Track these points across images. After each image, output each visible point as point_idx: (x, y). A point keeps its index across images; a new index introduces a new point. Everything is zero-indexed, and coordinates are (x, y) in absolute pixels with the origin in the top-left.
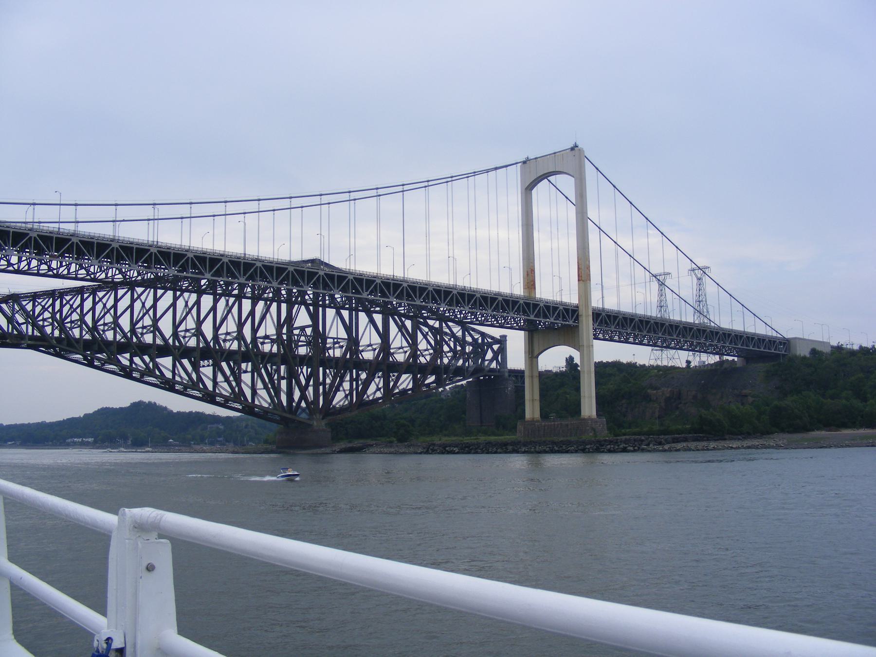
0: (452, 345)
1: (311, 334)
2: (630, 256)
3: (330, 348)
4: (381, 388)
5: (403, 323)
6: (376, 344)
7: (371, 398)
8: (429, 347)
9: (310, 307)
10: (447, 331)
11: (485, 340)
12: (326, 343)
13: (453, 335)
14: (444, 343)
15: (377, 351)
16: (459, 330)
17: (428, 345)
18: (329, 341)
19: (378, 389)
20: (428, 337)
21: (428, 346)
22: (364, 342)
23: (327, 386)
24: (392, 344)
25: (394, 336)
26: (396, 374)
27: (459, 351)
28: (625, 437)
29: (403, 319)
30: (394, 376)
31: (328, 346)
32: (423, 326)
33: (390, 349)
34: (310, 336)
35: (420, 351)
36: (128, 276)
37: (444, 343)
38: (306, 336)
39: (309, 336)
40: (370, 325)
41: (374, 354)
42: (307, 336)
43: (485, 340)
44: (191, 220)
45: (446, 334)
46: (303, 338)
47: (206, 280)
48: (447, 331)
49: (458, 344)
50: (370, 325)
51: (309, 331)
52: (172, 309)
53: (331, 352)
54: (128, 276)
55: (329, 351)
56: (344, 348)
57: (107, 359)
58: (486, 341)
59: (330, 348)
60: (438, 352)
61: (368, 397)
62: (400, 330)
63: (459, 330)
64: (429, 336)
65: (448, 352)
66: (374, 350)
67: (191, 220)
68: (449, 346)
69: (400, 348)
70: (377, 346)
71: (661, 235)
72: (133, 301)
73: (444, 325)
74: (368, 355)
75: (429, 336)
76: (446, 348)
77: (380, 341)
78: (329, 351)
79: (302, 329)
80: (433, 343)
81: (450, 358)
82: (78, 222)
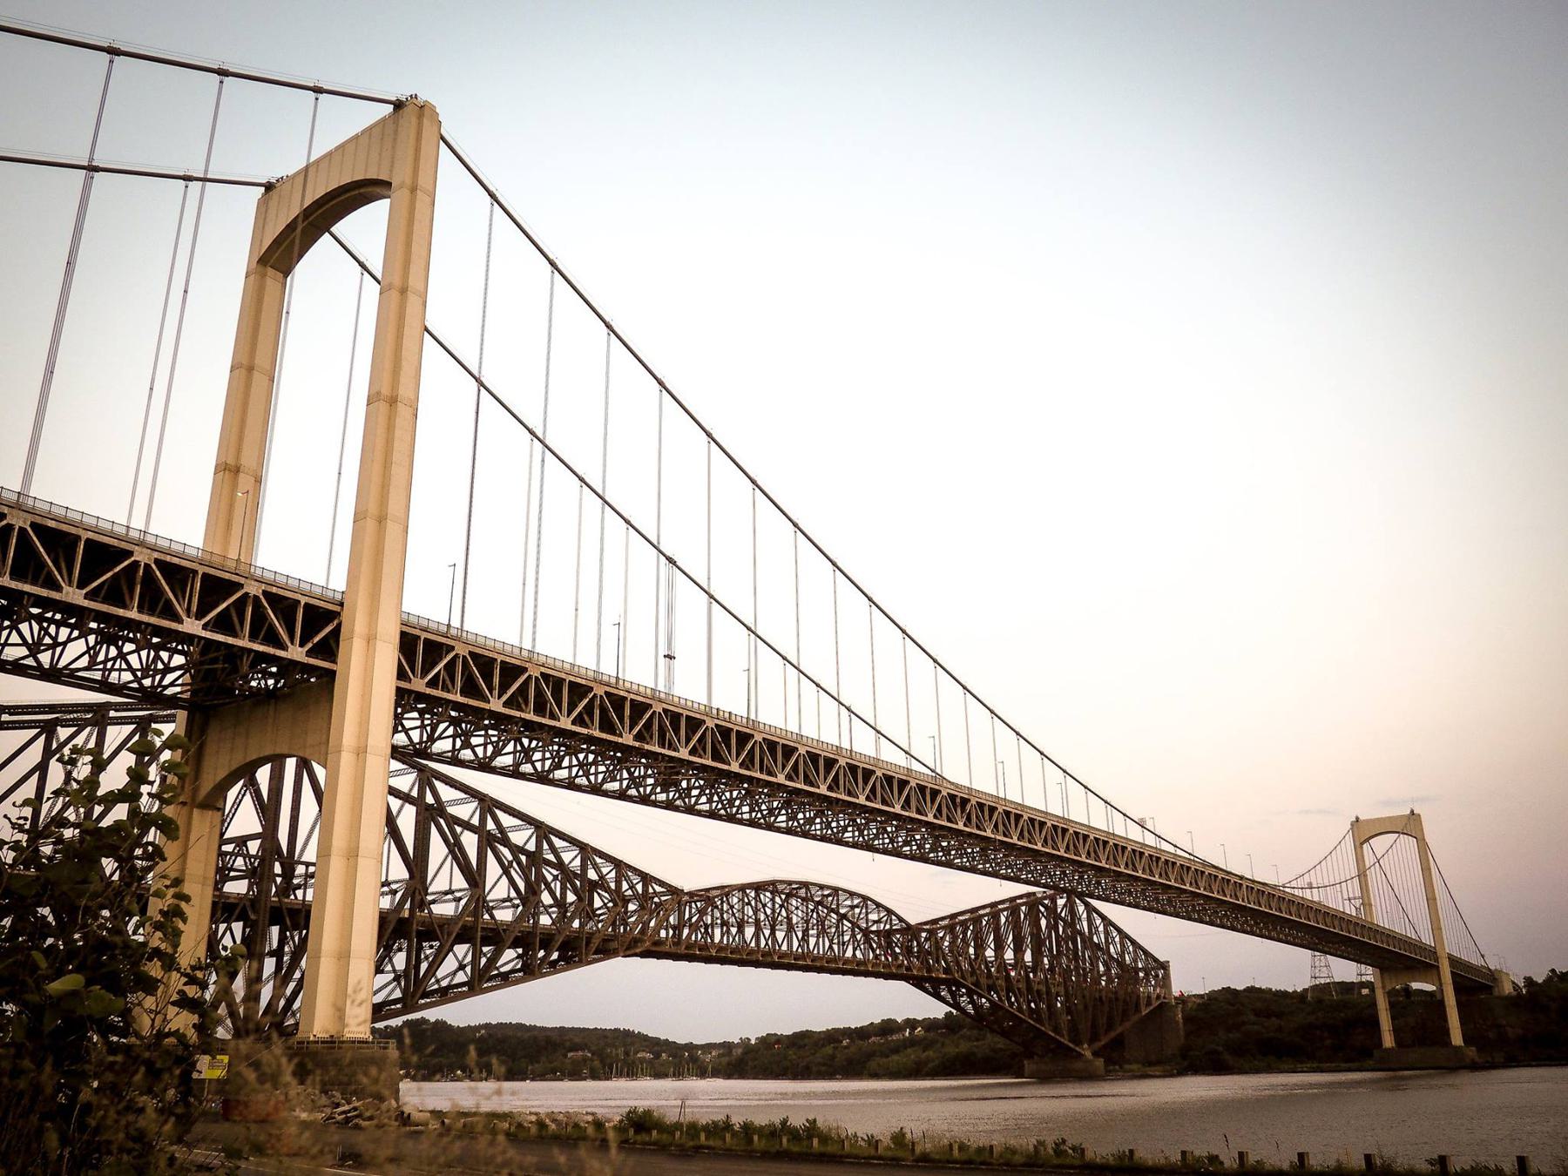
0: (557, 887)
1: (258, 852)
2: (749, 629)
3: (298, 887)
4: (465, 966)
5: (456, 837)
6: (397, 882)
7: (444, 983)
8: (513, 894)
9: (416, 796)
10: (551, 857)
11: (650, 888)
12: (293, 876)
13: (560, 865)
14: (543, 887)
15: (399, 895)
16: (576, 857)
17: (512, 890)
18: (300, 870)
19: (462, 967)
20: (513, 872)
21: (512, 890)
22: (438, 885)
23: (285, 958)
24: (488, 894)
25: (441, 871)
26: (436, 944)
27: (571, 904)
28: (1103, 1043)
29: (459, 829)
30: (431, 947)
31: (295, 881)
32: (501, 845)
33: (427, 894)
34: (255, 857)
35: (543, 906)
36: (50, 636)
37: (543, 887)
38: (247, 856)
39: (253, 856)
40: (390, 841)
41: (457, 907)
42: (250, 857)
43: (650, 888)
44: (206, 171)
45: (548, 863)
46: (240, 862)
47: (513, 742)
48: (551, 857)
49: (568, 885)
50: (390, 841)
51: (254, 847)
52: (36, 775)
53: (299, 893)
54: (50, 636)
55: (297, 892)
56: (399, 895)
57: (479, 970)
58: (651, 890)
59: (298, 887)
60: (529, 898)
61: (438, 981)
62: (451, 852)
63: (576, 857)
64: (514, 869)
65: (551, 906)
66: (394, 892)
67: (206, 171)
68: (552, 893)
69: (446, 893)
70: (398, 885)
71: (529, 436)
72: (48, 753)
73: (546, 846)
74: (445, 909)
75: (514, 869)
76: (546, 898)
77: (406, 875)
78: (297, 892)
79: (242, 841)
80: (521, 885)
81: (554, 916)
82: (97, 169)
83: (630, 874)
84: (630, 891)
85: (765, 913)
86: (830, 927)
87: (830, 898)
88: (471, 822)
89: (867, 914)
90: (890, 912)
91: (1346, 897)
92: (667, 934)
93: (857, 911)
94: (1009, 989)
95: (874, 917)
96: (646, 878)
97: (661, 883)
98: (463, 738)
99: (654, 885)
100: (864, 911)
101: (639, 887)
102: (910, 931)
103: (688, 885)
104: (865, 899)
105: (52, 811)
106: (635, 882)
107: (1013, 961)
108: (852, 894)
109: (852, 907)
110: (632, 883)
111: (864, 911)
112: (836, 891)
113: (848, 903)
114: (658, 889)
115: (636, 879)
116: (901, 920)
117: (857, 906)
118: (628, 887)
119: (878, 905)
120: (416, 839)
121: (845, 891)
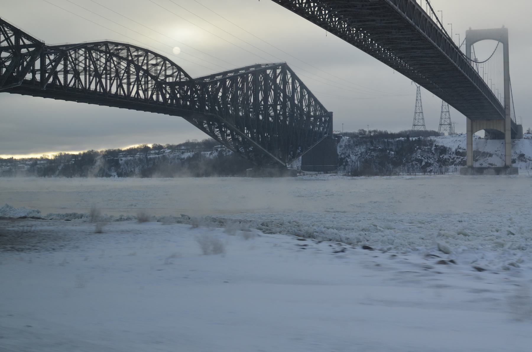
11: (21, 41)
43: (21, 41)
58: (21, 43)
83: (6, 29)
84: (6, 42)
85: (72, 58)
86: (100, 66)
87: (142, 58)
88: (170, 81)
89: (165, 70)
90: (180, 69)
91: (486, 74)
92: (224, 129)
93: (159, 68)
94: (313, 195)
95: (169, 72)
96: (19, 34)
97: (29, 38)
98: (281, 106)
99: (24, 39)
100: (163, 68)
101: (13, 39)
102: (191, 82)
103: (50, 41)
104: (165, 59)
105: (90, 80)
106: (9, 35)
107: (131, 77)
108: (157, 55)
109: (138, 56)
110: (8, 36)
111: (163, 68)
112: (147, 52)
113: (135, 54)
114: (27, 42)
115: (10, 33)
116: (186, 75)
117: (141, 56)
118: (4, 39)
119: (173, 64)
120: (15, 40)
121: (152, 53)
